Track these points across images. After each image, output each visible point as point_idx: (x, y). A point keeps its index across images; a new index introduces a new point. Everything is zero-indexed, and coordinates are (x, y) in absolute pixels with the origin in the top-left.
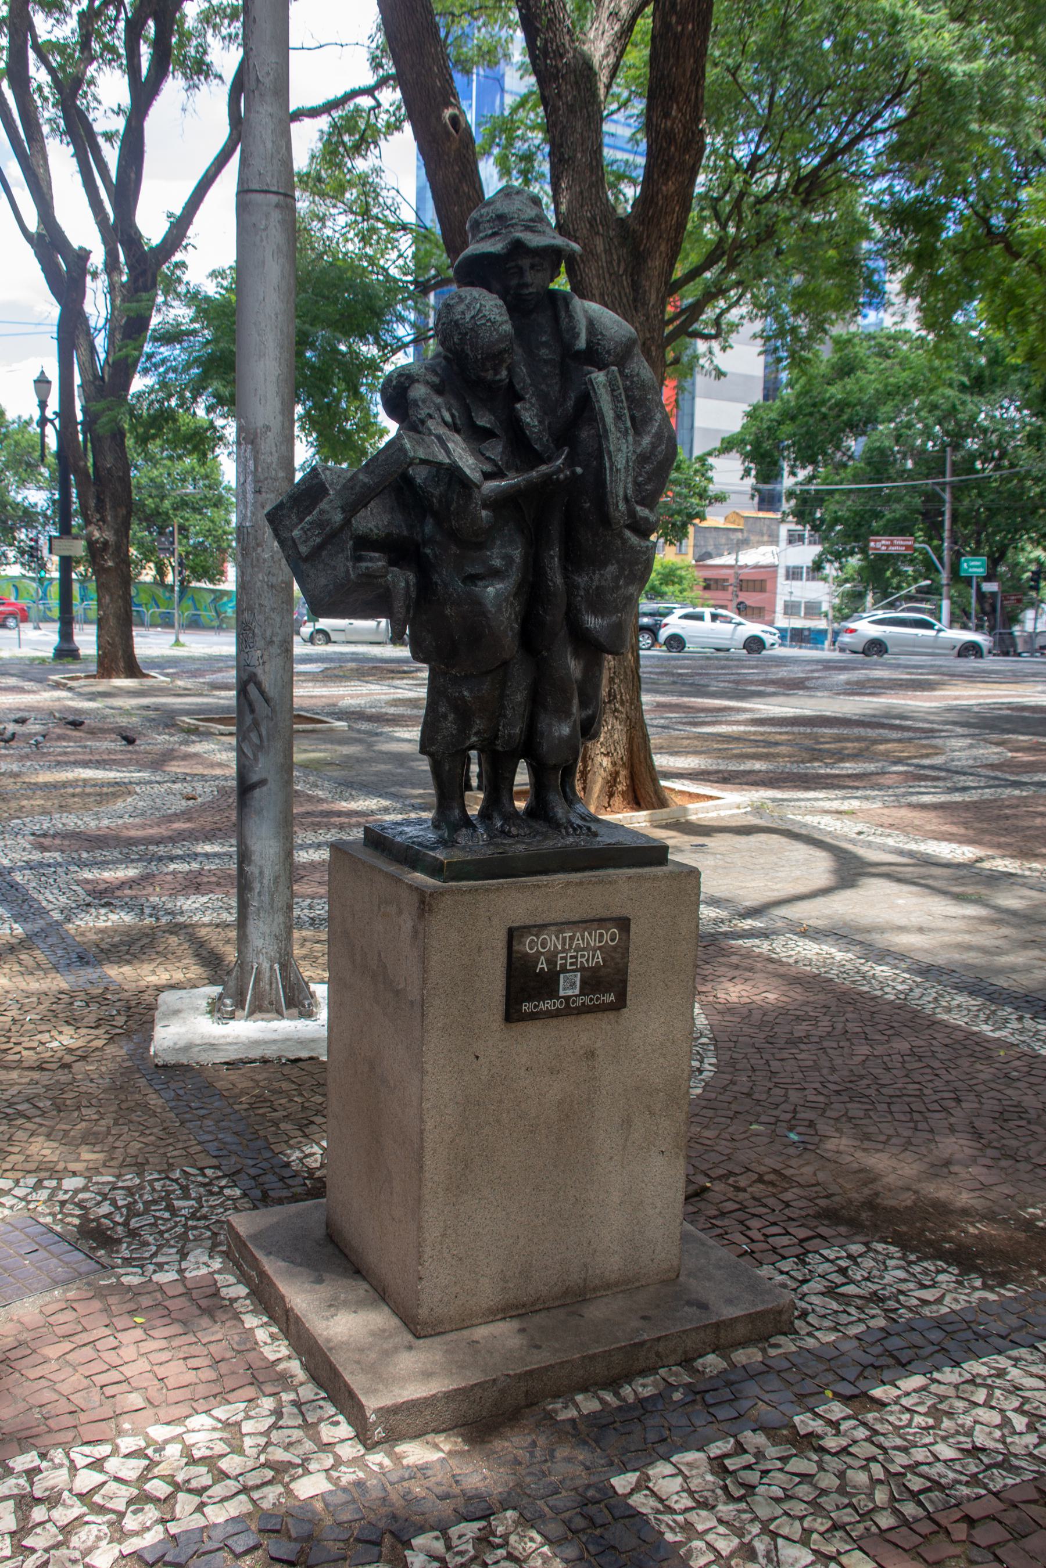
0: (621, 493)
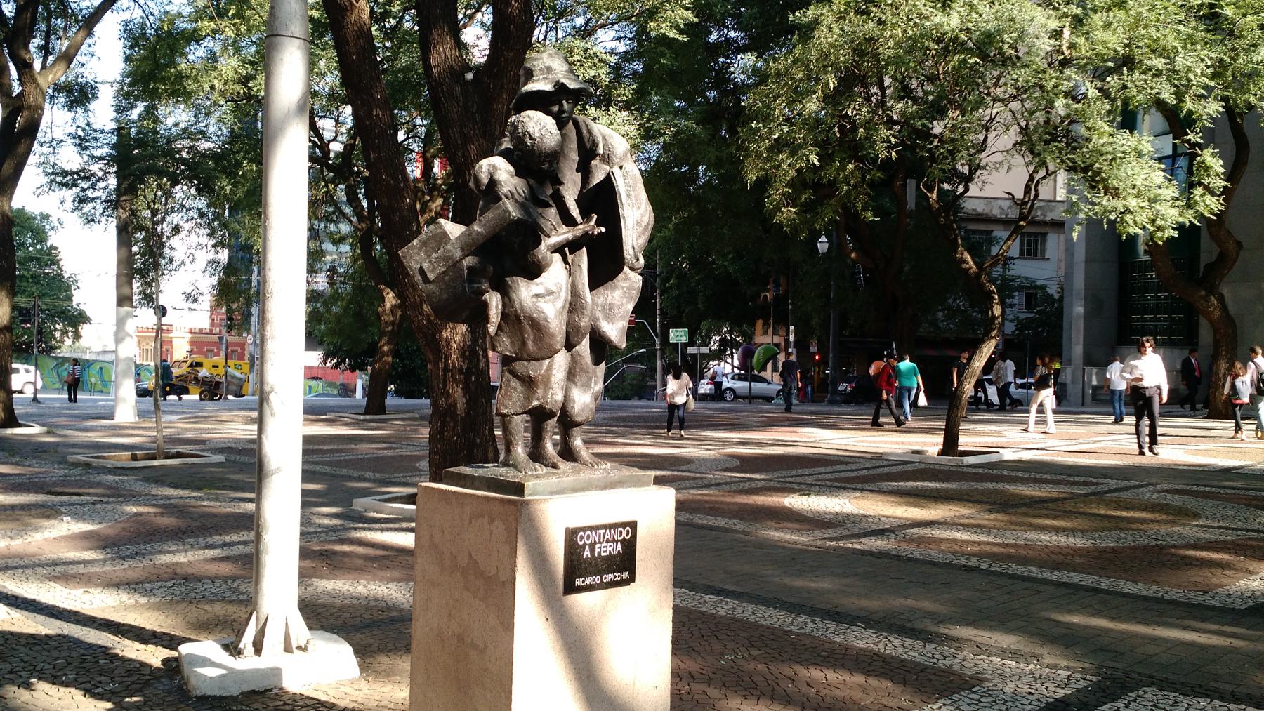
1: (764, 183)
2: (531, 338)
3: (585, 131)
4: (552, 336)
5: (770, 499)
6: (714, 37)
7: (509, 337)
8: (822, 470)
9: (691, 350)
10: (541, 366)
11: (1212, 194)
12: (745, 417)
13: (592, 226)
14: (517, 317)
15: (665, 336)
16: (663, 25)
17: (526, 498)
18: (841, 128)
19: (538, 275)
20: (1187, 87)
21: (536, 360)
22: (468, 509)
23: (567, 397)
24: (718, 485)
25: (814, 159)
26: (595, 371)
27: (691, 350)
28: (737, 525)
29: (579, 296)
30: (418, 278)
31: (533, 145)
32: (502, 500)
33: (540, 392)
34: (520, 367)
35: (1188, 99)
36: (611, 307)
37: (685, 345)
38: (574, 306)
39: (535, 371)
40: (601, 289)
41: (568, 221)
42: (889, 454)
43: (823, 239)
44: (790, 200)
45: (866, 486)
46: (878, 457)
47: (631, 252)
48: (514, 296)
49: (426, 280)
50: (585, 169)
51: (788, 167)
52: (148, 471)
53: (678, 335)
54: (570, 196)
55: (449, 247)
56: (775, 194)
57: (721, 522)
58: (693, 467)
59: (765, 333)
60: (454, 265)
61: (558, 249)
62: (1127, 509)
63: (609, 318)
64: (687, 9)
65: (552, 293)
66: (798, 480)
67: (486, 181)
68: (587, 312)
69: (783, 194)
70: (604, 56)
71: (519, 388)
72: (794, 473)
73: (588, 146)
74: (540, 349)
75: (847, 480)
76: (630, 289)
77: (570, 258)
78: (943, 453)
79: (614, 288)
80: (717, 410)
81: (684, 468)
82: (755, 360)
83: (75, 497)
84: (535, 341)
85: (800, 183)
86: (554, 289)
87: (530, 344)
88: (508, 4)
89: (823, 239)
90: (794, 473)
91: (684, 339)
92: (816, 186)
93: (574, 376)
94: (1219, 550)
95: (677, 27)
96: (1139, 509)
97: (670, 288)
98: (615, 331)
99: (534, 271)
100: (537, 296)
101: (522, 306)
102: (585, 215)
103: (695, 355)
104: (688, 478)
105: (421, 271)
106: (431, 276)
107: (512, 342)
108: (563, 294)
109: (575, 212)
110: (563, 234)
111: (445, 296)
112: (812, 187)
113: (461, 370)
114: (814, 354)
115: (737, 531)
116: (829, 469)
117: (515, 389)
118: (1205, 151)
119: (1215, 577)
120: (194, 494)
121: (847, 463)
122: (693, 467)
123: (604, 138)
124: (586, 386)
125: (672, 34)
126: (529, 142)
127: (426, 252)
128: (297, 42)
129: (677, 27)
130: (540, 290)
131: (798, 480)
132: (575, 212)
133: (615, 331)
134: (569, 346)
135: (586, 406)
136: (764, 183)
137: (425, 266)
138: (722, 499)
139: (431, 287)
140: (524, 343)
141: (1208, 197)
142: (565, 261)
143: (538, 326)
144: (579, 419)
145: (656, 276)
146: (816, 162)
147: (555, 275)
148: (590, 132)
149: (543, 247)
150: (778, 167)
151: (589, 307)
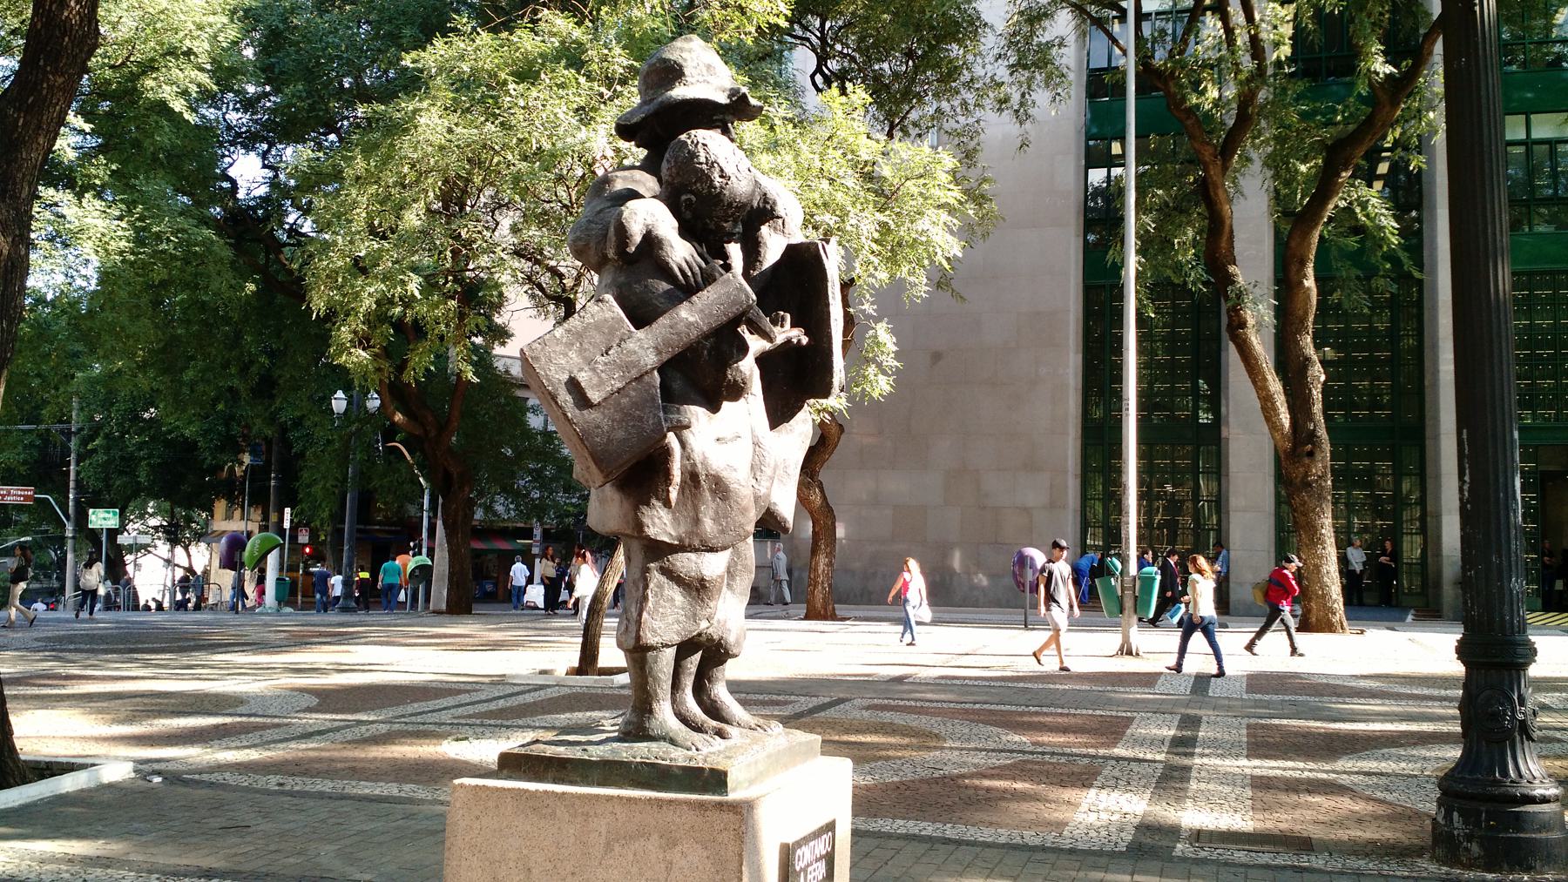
5: (414, 748)
11: (884, 373)
15: (82, 518)
16: (167, 88)
17: (732, 796)
18: (455, 253)
20: (856, 250)
22: (601, 825)
24: (320, 733)
30: (565, 398)
32: (688, 803)
35: (857, 265)
42: (514, 677)
43: (340, 394)
44: (363, 341)
45: (529, 721)
46: (500, 681)
49: (582, 401)
53: (102, 519)
56: (345, 333)
57: (392, 789)
59: (229, 517)
60: (639, 379)
62: (858, 732)
64: (201, 69)
66: (435, 718)
67: (638, 239)
75: (500, 714)
78: (579, 671)
81: (239, 710)
82: (246, 554)
85: (378, 317)
88: (63, 3)
89: (340, 394)
94: (1000, 777)
95: (185, 93)
96: (876, 732)
97: (94, 451)
104: (264, 727)
105: (574, 385)
106: (595, 396)
111: (620, 434)
114: (305, 545)
115: (422, 802)
118: (879, 325)
119: (1029, 810)
121: (459, 692)
126: (717, 180)
131: (435, 718)
137: (583, 377)
138: (336, 754)
139: (591, 415)
140: (697, 521)
141: (881, 377)
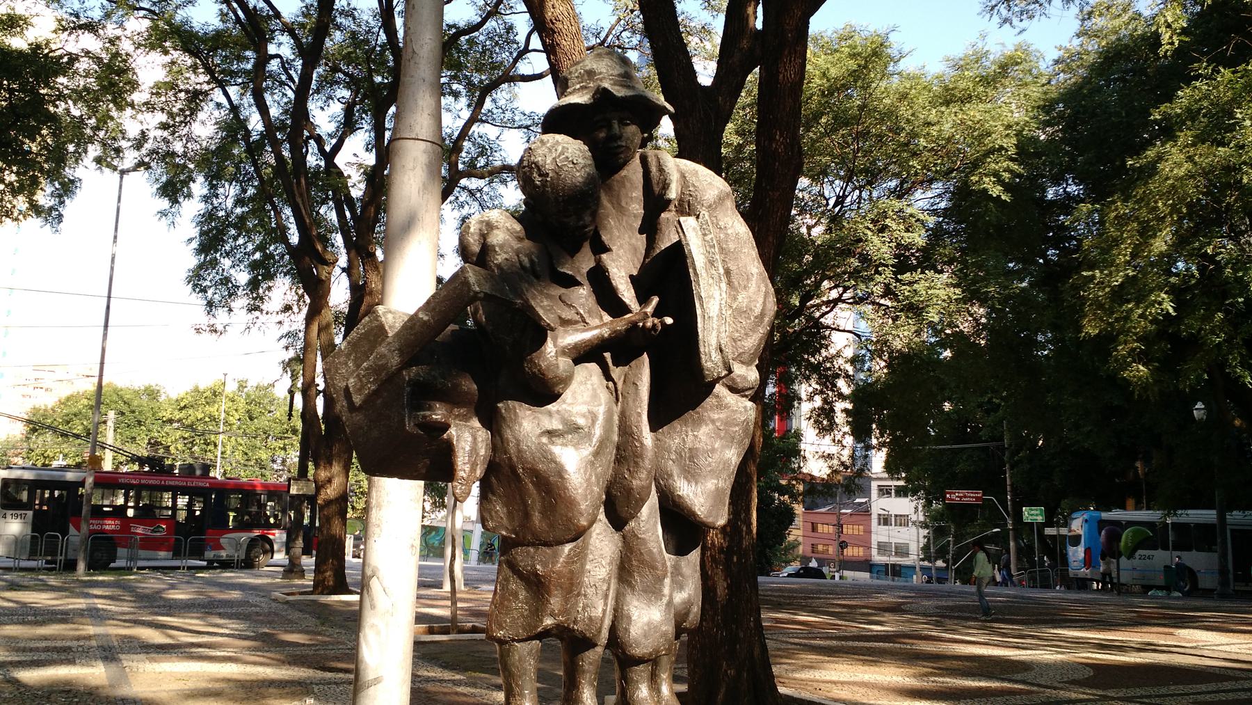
0: (714, 342)
1: (1107, 340)
2: (538, 505)
3: (654, 169)
4: (571, 503)
6: (1050, 194)
7: (506, 505)
8: (1203, 688)
9: (1049, 531)
10: (556, 556)
12: (1110, 612)
13: (642, 312)
14: (513, 469)
15: (1018, 515)
16: (986, 180)
19: (555, 397)
21: (547, 544)
23: (619, 615)
25: (1169, 307)
26: (677, 570)
27: (1049, 531)
28: (1158, 701)
29: (631, 434)
31: (544, 183)
33: (555, 602)
34: (522, 555)
36: (693, 454)
37: (1041, 526)
38: (625, 451)
39: (545, 565)
40: (676, 423)
41: (613, 304)
47: (716, 357)
48: (508, 434)
50: (650, 227)
51: (1139, 317)
52: (432, 647)
53: (1033, 514)
54: (621, 269)
55: (383, 349)
58: (1029, 676)
61: (583, 355)
63: (691, 474)
65: (576, 429)
68: (647, 463)
69: (1133, 350)
70: (921, 217)
71: (522, 594)
72: (1163, 691)
73: (657, 189)
74: (551, 526)
76: (728, 423)
77: (616, 372)
79: (699, 422)
80: (1076, 601)
81: (1019, 677)
82: (1122, 544)
83: (341, 675)
84: (543, 513)
86: (581, 421)
87: (536, 517)
90: (1163, 691)
91: (1040, 519)
92: (1175, 339)
93: (630, 574)
98: (704, 496)
99: (543, 392)
100: (550, 433)
101: (519, 451)
102: (643, 299)
103: (1054, 536)
106: (357, 399)
107: (510, 514)
108: (598, 432)
109: (627, 294)
110: (599, 326)
112: (1169, 343)
113: (721, 549)
116: (1212, 686)
117: (515, 595)
120: (458, 677)
122: (1029, 676)
123: (683, 176)
124: (653, 592)
125: (996, 191)
127: (355, 361)
128: (422, 145)
129: (1000, 181)
130: (556, 425)
132: (627, 294)
133: (704, 496)
134: (618, 520)
135: (651, 627)
136: (1107, 340)
140: (527, 515)
142: (608, 377)
143: (549, 486)
144: (638, 651)
145: (1003, 449)
146: (1171, 310)
147: (586, 395)
148: (661, 170)
149: (550, 348)
150: (1127, 319)
151: (649, 454)
